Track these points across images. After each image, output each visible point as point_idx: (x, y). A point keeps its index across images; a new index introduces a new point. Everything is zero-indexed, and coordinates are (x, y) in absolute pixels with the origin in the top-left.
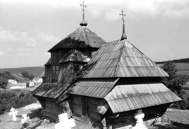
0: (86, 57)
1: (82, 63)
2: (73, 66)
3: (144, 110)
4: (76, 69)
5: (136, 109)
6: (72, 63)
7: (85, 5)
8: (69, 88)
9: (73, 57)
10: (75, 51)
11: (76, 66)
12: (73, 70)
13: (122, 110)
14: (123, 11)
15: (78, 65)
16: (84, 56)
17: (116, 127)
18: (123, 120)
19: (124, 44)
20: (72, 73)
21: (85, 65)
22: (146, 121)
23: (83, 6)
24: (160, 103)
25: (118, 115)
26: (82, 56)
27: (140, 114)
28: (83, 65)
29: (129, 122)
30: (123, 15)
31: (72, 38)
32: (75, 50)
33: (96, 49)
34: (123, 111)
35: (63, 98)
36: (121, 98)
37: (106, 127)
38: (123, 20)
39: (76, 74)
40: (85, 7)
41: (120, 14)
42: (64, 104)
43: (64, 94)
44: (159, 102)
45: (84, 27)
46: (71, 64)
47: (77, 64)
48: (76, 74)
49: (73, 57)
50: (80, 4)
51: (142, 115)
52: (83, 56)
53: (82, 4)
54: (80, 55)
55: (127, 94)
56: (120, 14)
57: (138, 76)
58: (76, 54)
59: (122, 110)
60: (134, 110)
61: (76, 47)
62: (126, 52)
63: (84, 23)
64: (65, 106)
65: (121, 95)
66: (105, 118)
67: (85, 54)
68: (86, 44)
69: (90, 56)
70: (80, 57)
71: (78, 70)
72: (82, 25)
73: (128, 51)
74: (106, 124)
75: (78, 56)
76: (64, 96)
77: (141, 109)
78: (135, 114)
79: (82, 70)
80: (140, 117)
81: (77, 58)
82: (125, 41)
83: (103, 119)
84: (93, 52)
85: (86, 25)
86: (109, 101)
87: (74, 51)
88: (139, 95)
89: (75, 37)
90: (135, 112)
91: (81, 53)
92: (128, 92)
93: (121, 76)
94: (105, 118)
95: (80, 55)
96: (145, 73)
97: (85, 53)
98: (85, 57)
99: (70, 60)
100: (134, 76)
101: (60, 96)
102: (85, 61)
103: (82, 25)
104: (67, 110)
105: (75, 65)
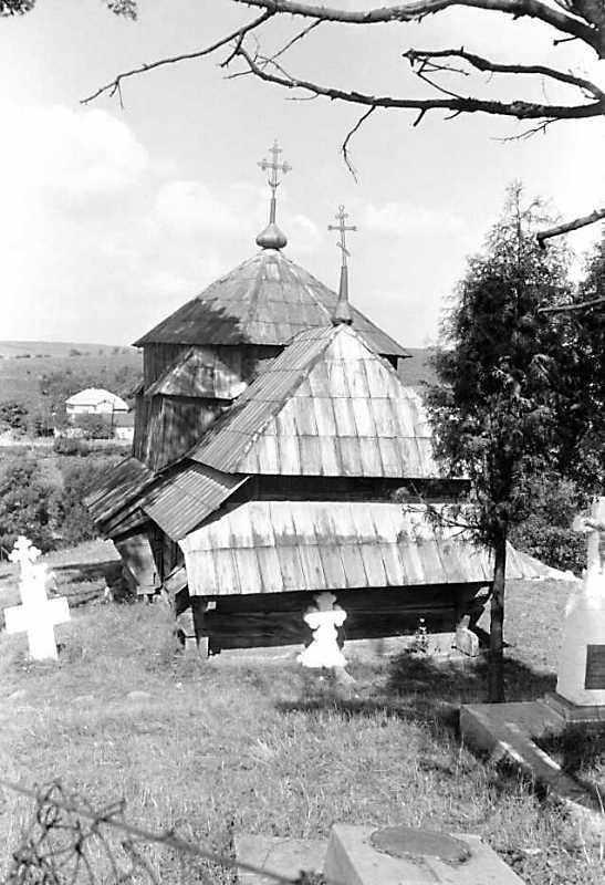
0: (234, 377)
1: (212, 402)
2: (172, 411)
3: (344, 597)
4: (187, 423)
5: (288, 590)
6: (170, 402)
7: (280, 163)
8: (151, 490)
9: (177, 380)
10: (195, 357)
11: (188, 411)
12: (170, 428)
13: (227, 590)
14: (345, 211)
15: (194, 409)
16: (226, 374)
17: (237, 642)
18: (267, 623)
19: (327, 346)
20: (168, 434)
21: (225, 409)
22: (376, 641)
23: (275, 167)
24: (416, 580)
25: (212, 605)
26: (220, 374)
27: (324, 611)
28: (213, 410)
29: (291, 633)
30: (342, 230)
31: (204, 303)
32: (196, 351)
33: (276, 350)
34: (362, 585)
35: (127, 525)
36: (245, 545)
37: (195, 640)
38: (344, 250)
39: (183, 440)
40: (280, 171)
41: (330, 228)
42: (133, 546)
43: (132, 509)
44: (414, 574)
45: (271, 252)
46: (167, 404)
47: (191, 406)
48: (183, 440)
49: (177, 380)
50: (261, 160)
51: (340, 616)
52: (222, 375)
53: (270, 161)
54: (209, 372)
55: (281, 534)
56: (330, 228)
57: (337, 474)
58: (193, 370)
59: (227, 589)
60: (278, 593)
61: (199, 342)
62: (326, 375)
63: (271, 236)
64: (137, 552)
65: (248, 538)
66: (190, 609)
67: (231, 369)
68: (237, 329)
69: (248, 376)
70: (209, 378)
71: (193, 427)
72: (265, 244)
73: (337, 375)
74: (196, 631)
75: (200, 376)
76: (134, 516)
77: (329, 594)
78: (309, 609)
79: (210, 428)
80: (326, 620)
81: (193, 384)
82: (336, 333)
83: (183, 611)
84: (261, 362)
85: (278, 245)
86: (189, 553)
87: (191, 355)
88: (328, 543)
89: (216, 299)
90: (307, 599)
91: (217, 362)
92: (286, 528)
93: (255, 472)
94: (190, 609)
95: (212, 369)
96: (370, 464)
97: (231, 362)
98: (227, 379)
99: (164, 390)
100: (318, 474)
101: (114, 516)
102: (225, 395)
103: (265, 244)
104: (145, 566)
105: (183, 409)
